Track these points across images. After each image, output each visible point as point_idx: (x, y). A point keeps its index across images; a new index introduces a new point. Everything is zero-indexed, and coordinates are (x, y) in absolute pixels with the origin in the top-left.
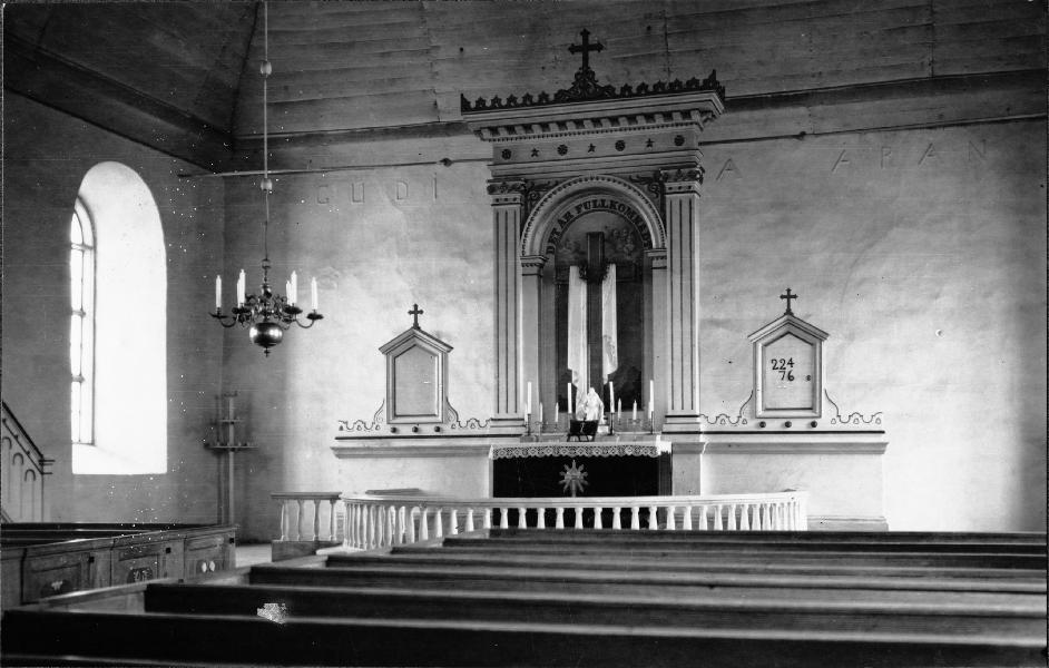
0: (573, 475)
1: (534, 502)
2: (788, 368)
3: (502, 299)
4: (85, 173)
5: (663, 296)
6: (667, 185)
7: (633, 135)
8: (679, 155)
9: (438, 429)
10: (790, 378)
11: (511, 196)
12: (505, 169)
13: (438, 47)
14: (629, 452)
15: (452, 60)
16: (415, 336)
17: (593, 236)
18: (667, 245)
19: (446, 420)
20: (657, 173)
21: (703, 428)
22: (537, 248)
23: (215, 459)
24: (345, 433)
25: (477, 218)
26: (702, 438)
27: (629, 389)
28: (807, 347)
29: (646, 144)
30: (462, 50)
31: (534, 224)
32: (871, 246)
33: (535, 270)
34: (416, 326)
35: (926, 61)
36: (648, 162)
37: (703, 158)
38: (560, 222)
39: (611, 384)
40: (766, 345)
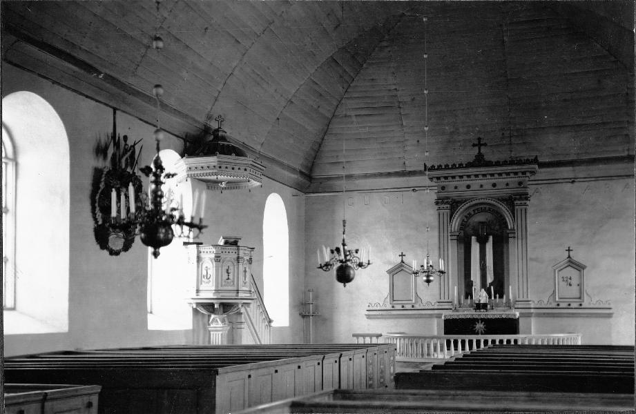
0: (480, 326)
1: (463, 337)
2: (569, 281)
3: (442, 250)
4: (266, 199)
5: (514, 251)
6: (515, 202)
7: (501, 181)
8: (521, 191)
9: (413, 306)
10: (570, 285)
11: (445, 206)
12: (443, 194)
13: (407, 140)
14: (504, 317)
15: (414, 145)
16: (402, 266)
17: (482, 223)
18: (516, 228)
19: (416, 302)
20: (510, 197)
21: (532, 306)
22: (456, 227)
23: (302, 319)
24: (371, 308)
25: (431, 215)
26: (532, 311)
27: (499, 287)
28: (578, 272)
29: (505, 183)
30: (418, 141)
31: (456, 218)
32: (601, 227)
33: (455, 237)
34: (402, 261)
35: (626, 148)
36: (506, 192)
37: (530, 191)
38: (466, 217)
39: (492, 287)
40: (560, 271)
